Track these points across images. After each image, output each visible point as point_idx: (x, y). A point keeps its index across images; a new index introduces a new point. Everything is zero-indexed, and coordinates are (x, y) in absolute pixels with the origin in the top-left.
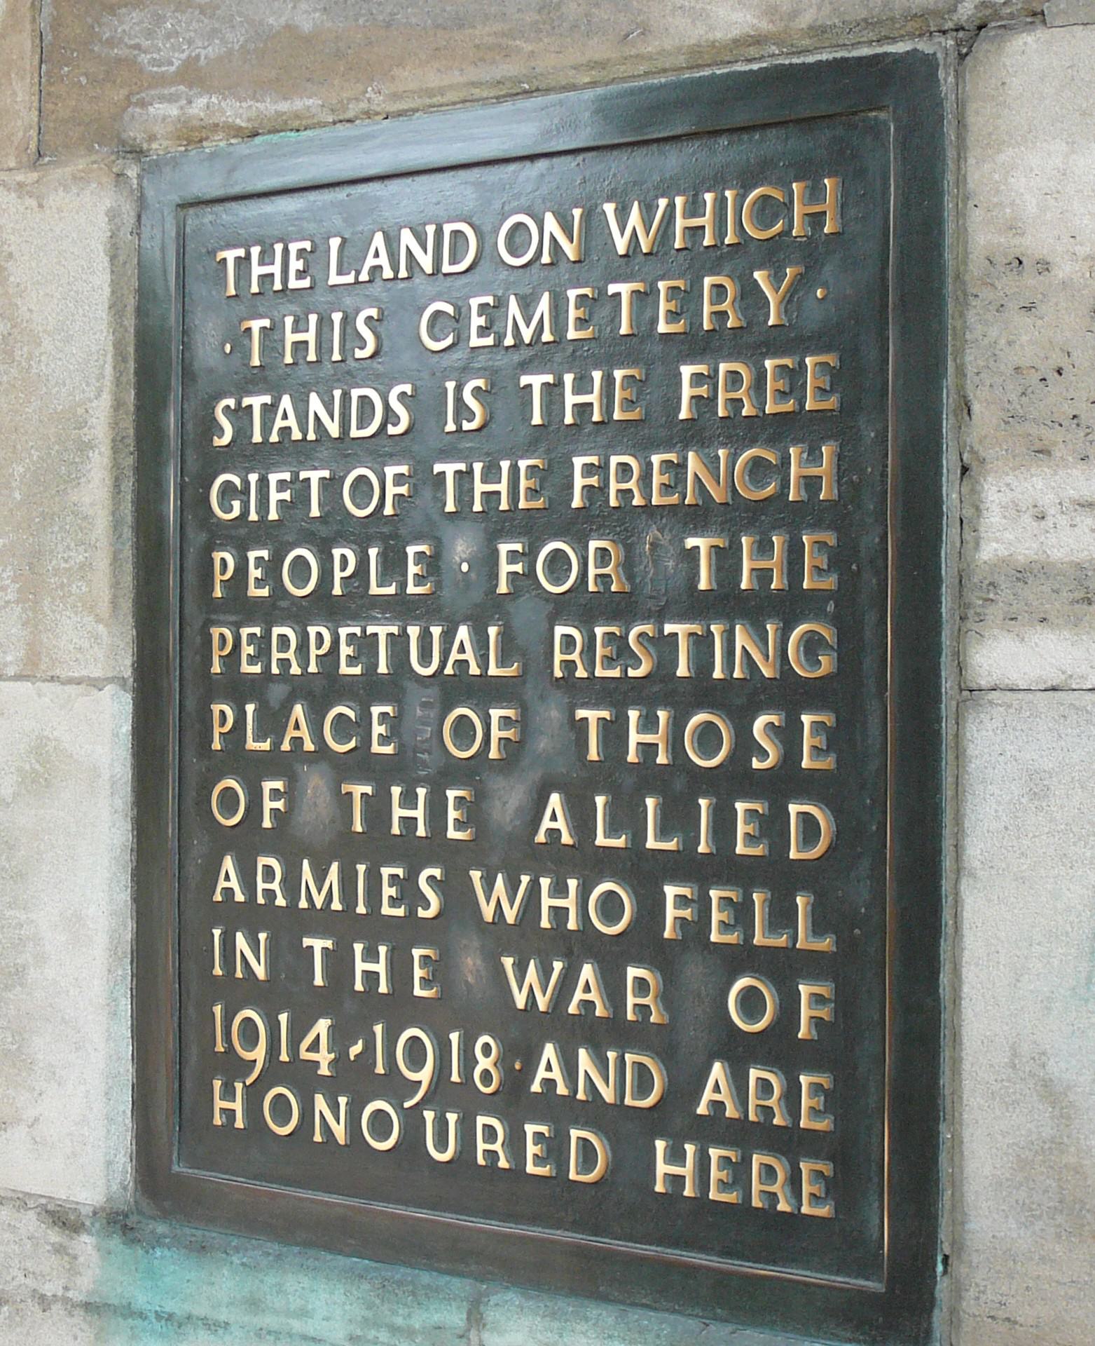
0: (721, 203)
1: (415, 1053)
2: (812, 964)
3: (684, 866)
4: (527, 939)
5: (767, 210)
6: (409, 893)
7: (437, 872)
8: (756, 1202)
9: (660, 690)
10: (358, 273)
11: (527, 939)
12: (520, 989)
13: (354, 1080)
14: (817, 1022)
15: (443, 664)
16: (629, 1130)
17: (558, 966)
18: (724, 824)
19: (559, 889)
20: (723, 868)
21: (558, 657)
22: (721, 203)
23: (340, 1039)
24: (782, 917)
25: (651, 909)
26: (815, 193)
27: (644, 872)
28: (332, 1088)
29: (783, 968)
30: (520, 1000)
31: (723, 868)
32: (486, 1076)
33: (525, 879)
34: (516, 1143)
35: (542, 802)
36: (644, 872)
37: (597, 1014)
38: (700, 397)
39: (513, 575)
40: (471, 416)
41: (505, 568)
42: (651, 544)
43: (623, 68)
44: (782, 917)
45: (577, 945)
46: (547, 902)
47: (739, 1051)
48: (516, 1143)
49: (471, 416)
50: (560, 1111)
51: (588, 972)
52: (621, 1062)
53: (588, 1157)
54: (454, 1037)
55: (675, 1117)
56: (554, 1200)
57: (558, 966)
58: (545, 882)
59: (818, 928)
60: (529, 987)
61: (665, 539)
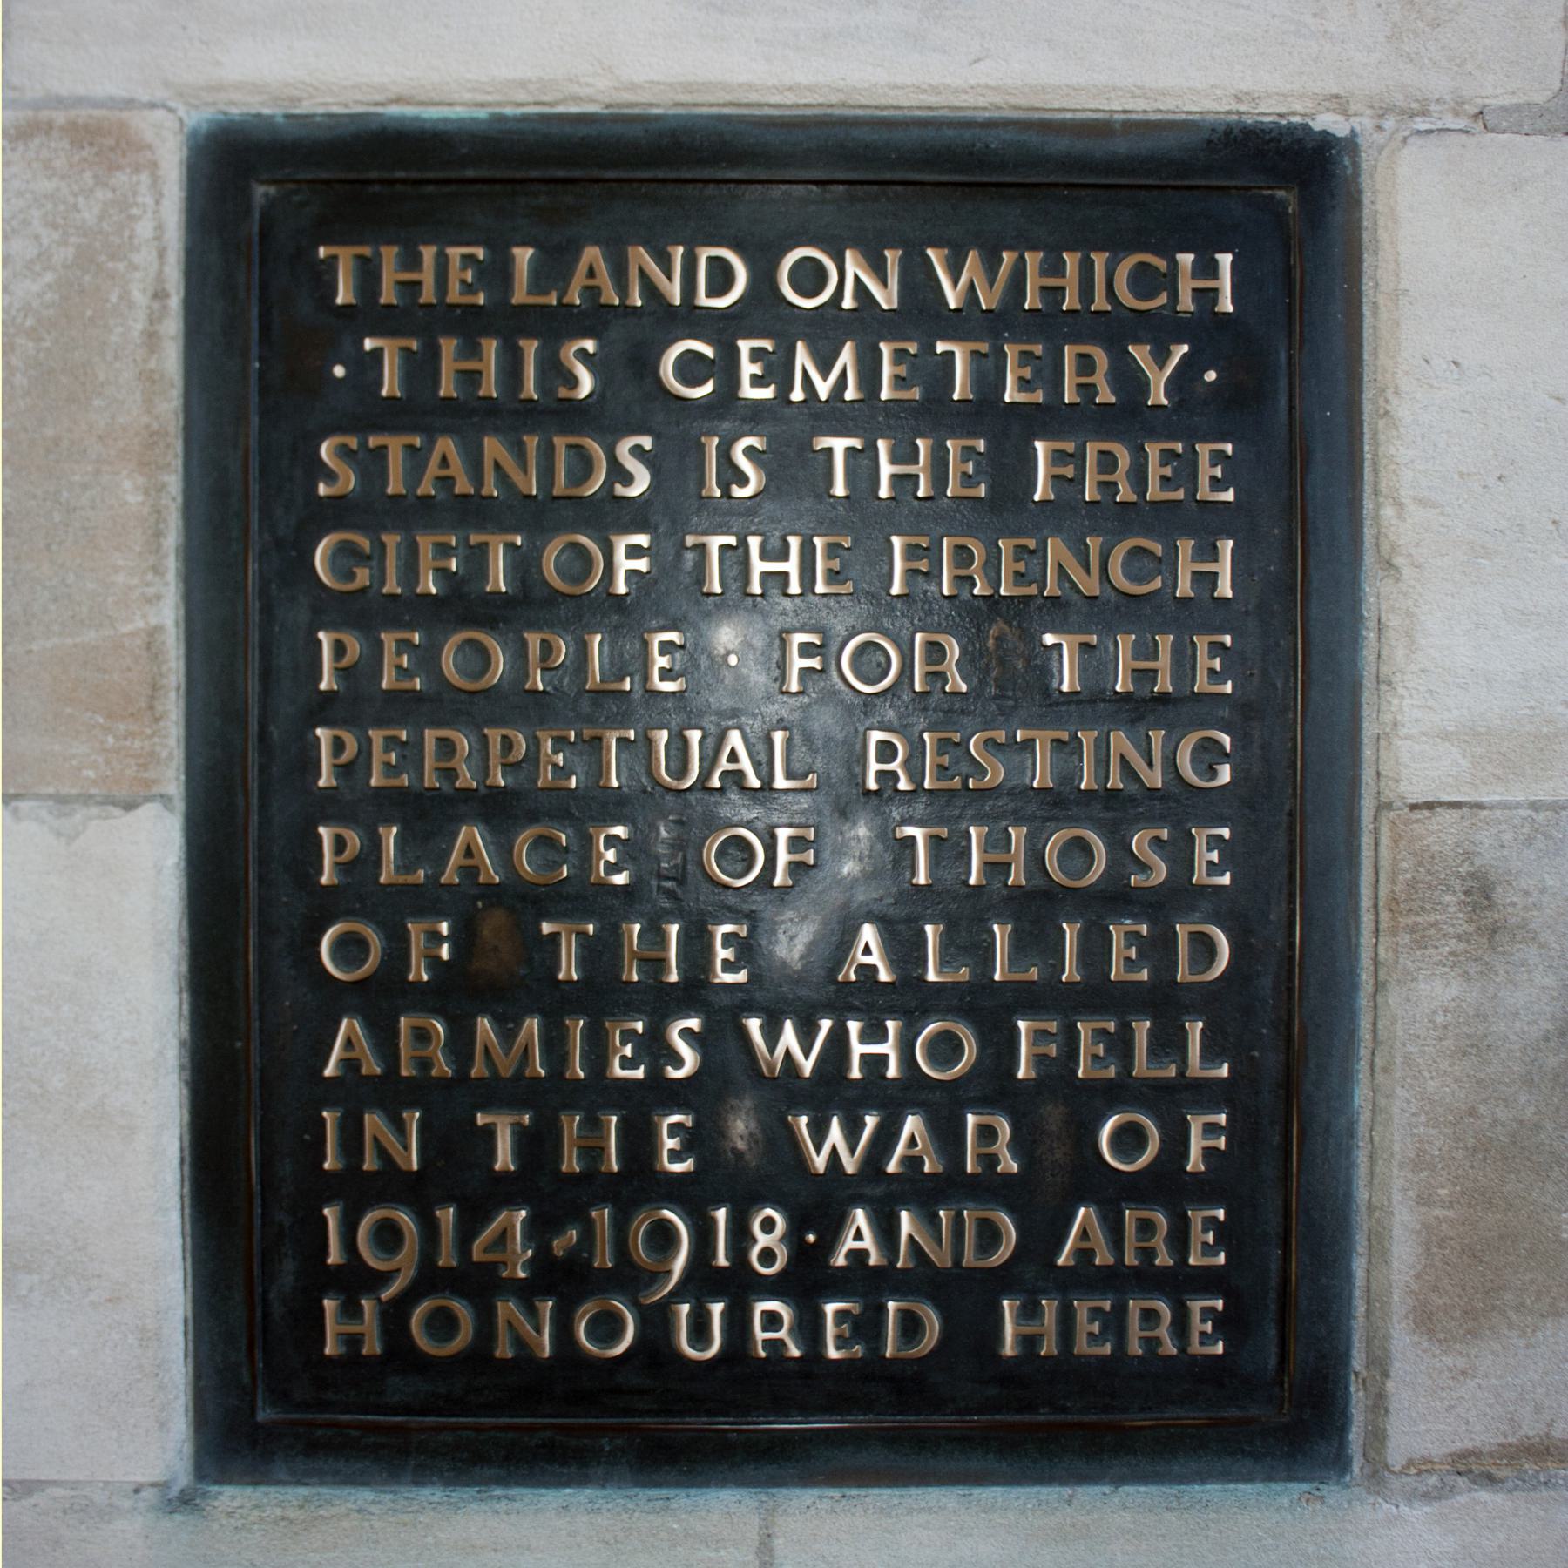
0: (1087, 267)
1: (388, 1236)
2: (1203, 1093)
3: (1028, 999)
4: (831, 1091)
5: (1144, 281)
6: (656, 1049)
7: (694, 1023)
8: (1135, 1348)
9: (1060, 803)
10: (563, 293)
11: (831, 1091)
12: (834, 1149)
13: (562, 1279)
14: (1208, 1153)
15: (705, 775)
16: (966, 1295)
17: (871, 1121)
18: (1095, 950)
19: (874, 1033)
20: (1098, 995)
21: (874, 766)
22: (1087, 267)
23: (539, 1229)
24: (1168, 1042)
25: (1000, 1046)
26: (1208, 268)
27: (989, 1009)
28: (527, 1293)
29: (1172, 1100)
30: (820, 1162)
31: (1098, 995)
32: (767, 1256)
33: (826, 1025)
34: (810, 1328)
35: (851, 933)
36: (989, 1009)
37: (365, 1167)
38: (1063, 477)
39: (805, 673)
40: (743, 480)
41: (798, 663)
42: (996, 639)
43: (964, 97)
44: (1168, 1042)
45: (889, 1096)
46: (858, 1049)
47: (1112, 1193)
48: (810, 1328)
49: (743, 480)
50: (865, 1281)
51: (912, 1124)
52: (958, 1222)
53: (912, 1330)
54: (721, 1215)
55: (1032, 1272)
56: (868, 1382)
57: (871, 1121)
58: (854, 1027)
59: (1211, 1053)
60: (834, 1147)
61: (1012, 636)
